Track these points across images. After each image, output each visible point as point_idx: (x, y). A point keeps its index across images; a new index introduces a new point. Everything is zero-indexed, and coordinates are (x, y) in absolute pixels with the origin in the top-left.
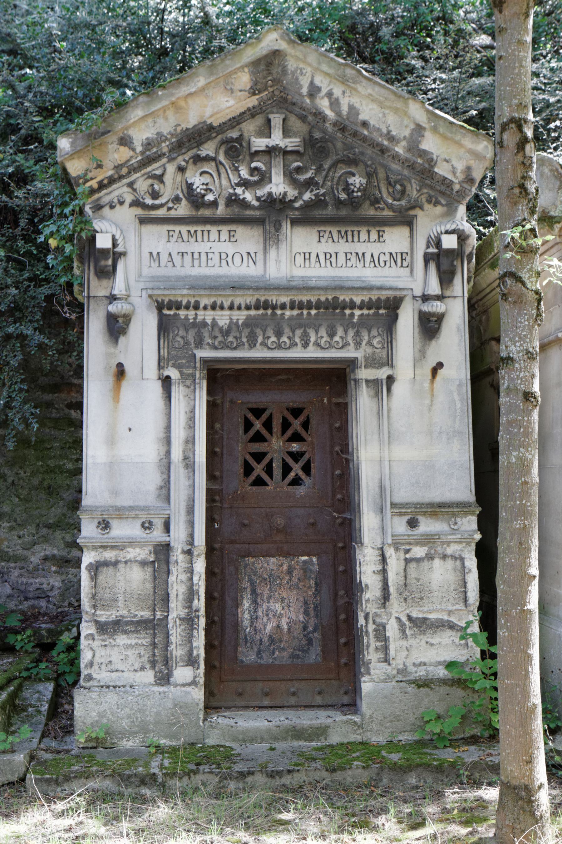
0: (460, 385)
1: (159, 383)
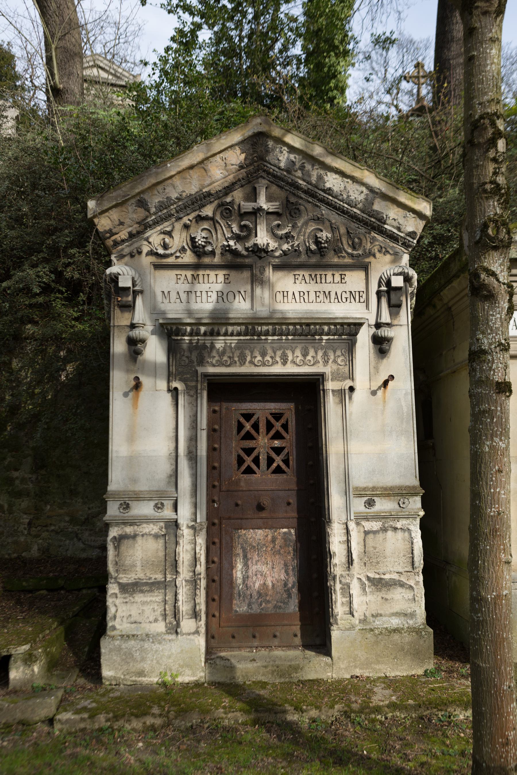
0: (406, 394)
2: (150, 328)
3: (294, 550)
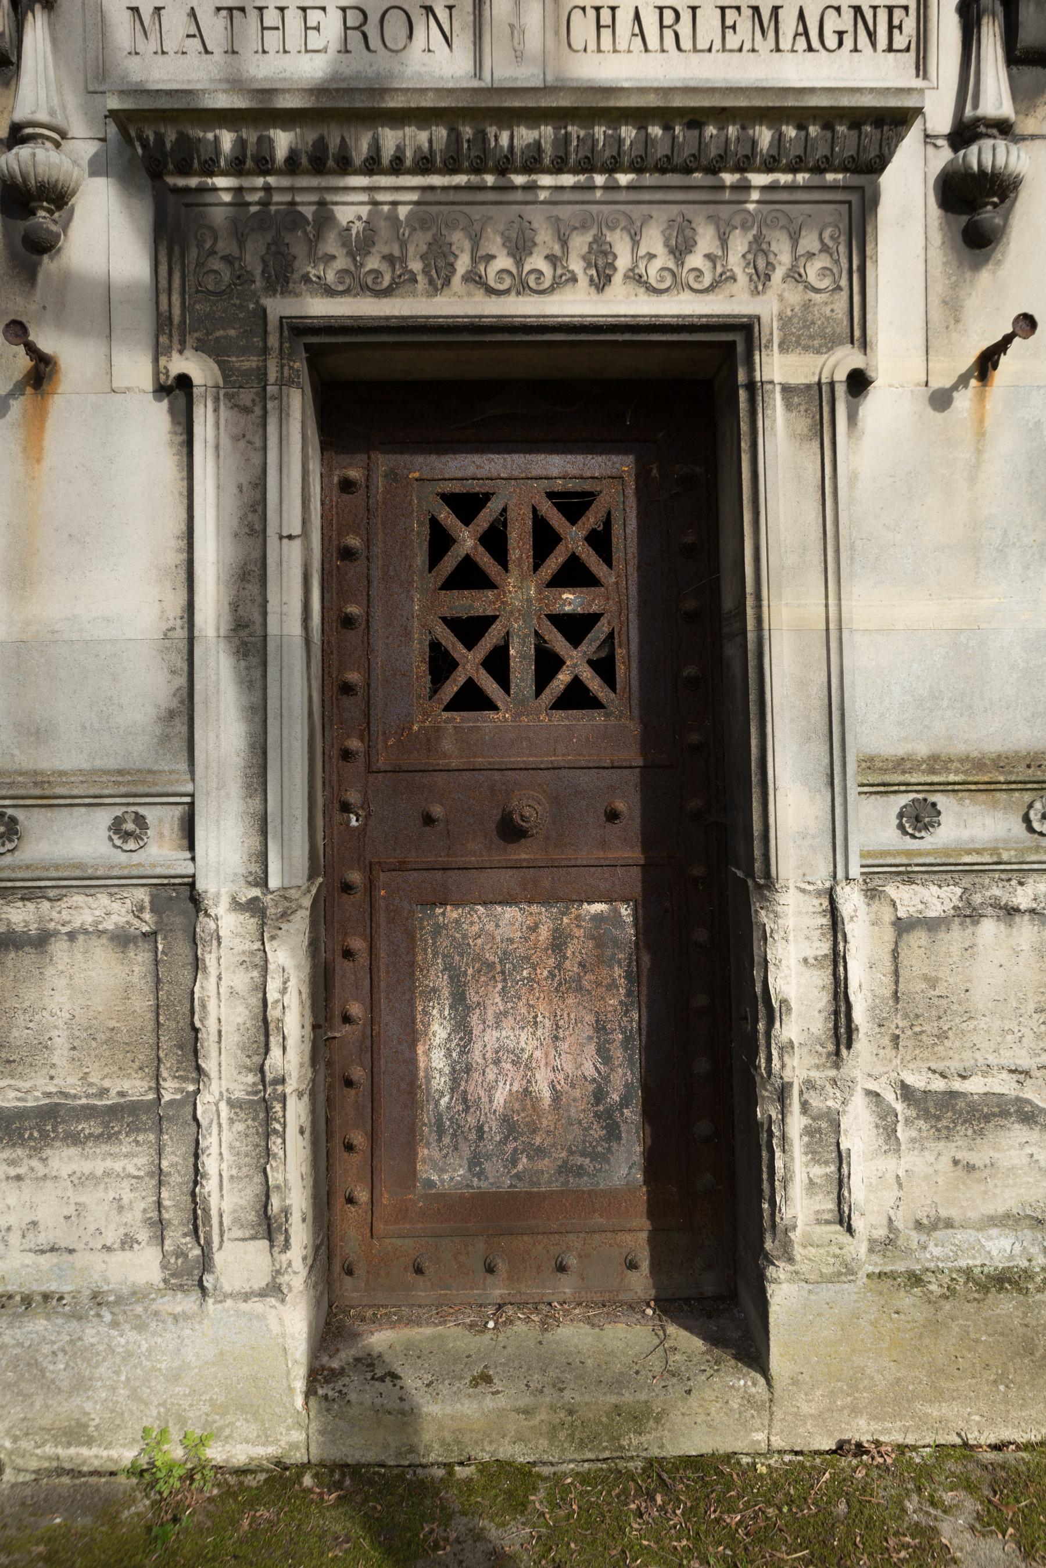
2: (84, 148)
3: (628, 976)
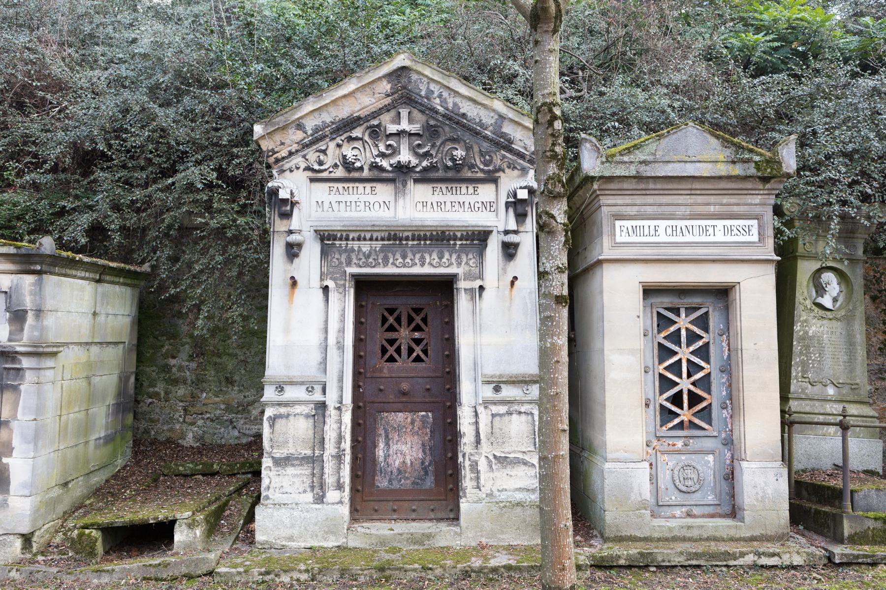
0: (530, 293)
1: (321, 290)
